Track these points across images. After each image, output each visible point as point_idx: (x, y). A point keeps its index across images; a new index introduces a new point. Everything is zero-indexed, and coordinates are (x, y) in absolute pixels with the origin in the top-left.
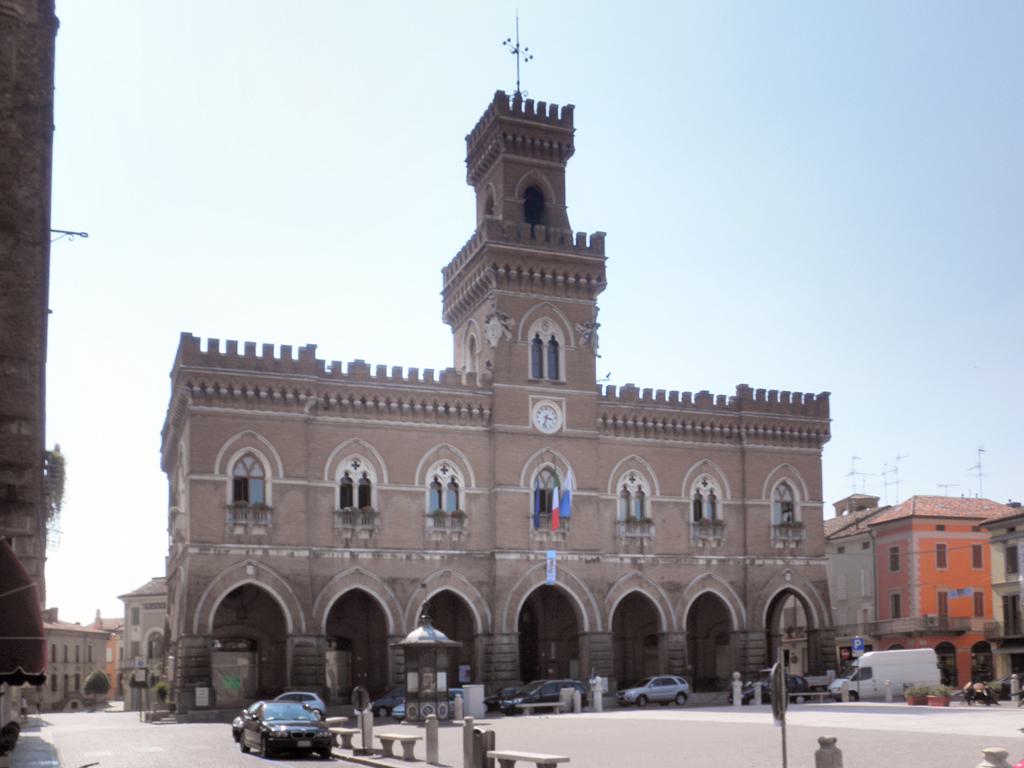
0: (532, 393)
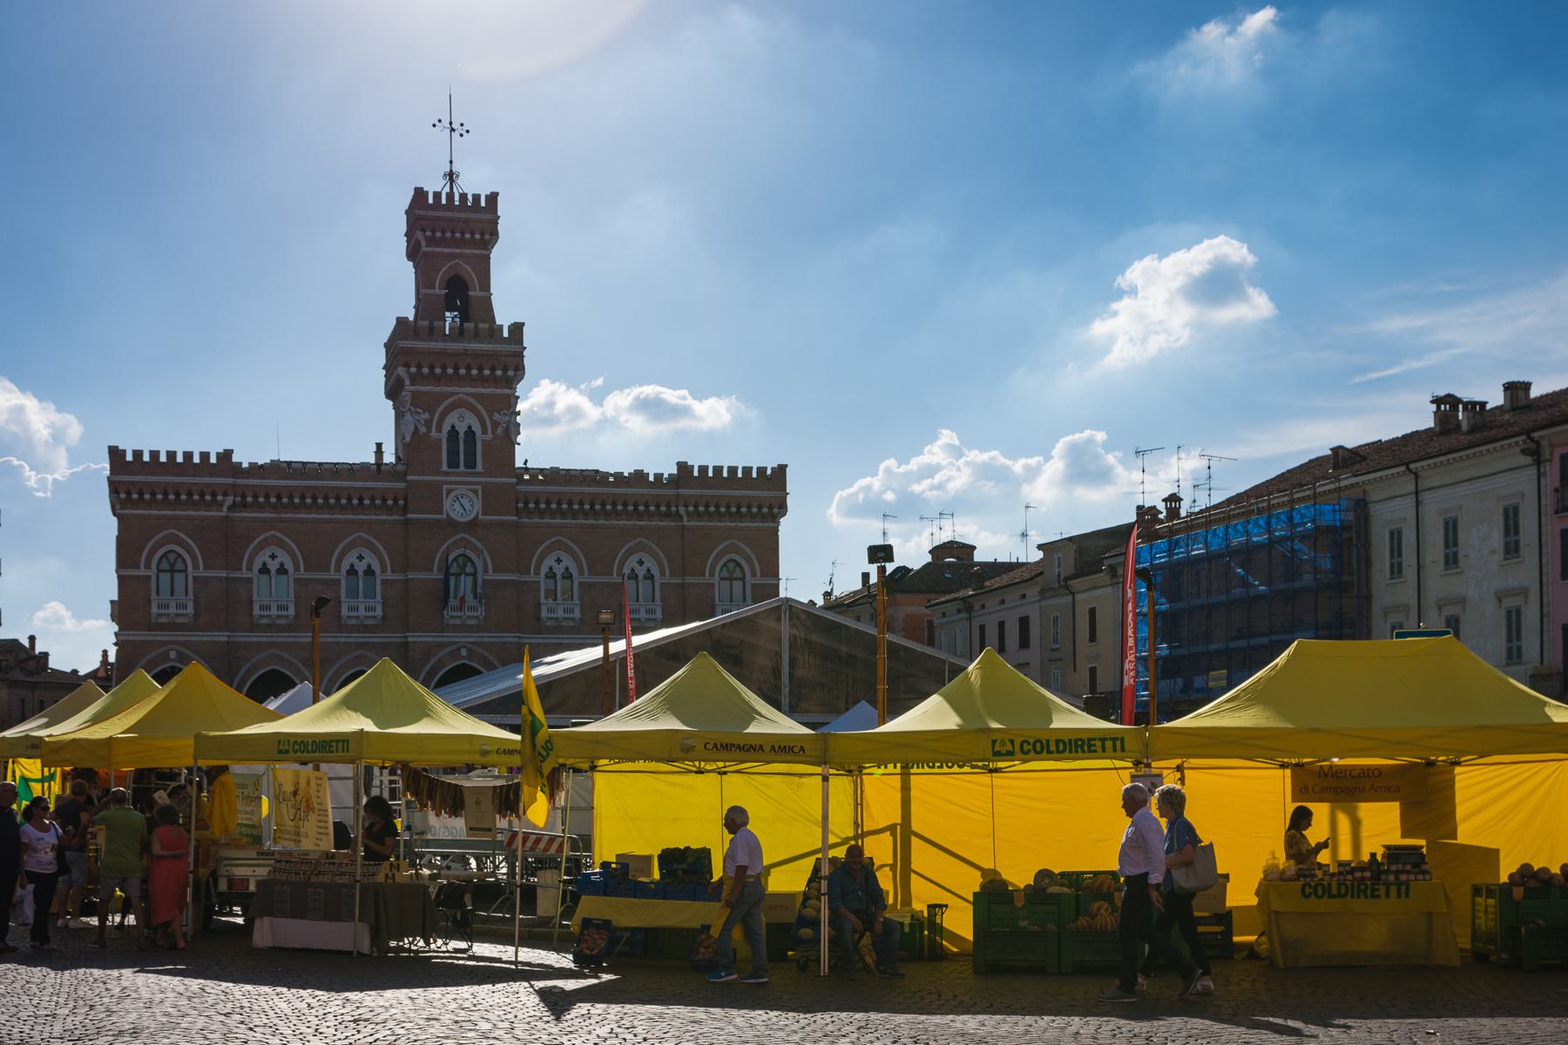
0: (447, 483)
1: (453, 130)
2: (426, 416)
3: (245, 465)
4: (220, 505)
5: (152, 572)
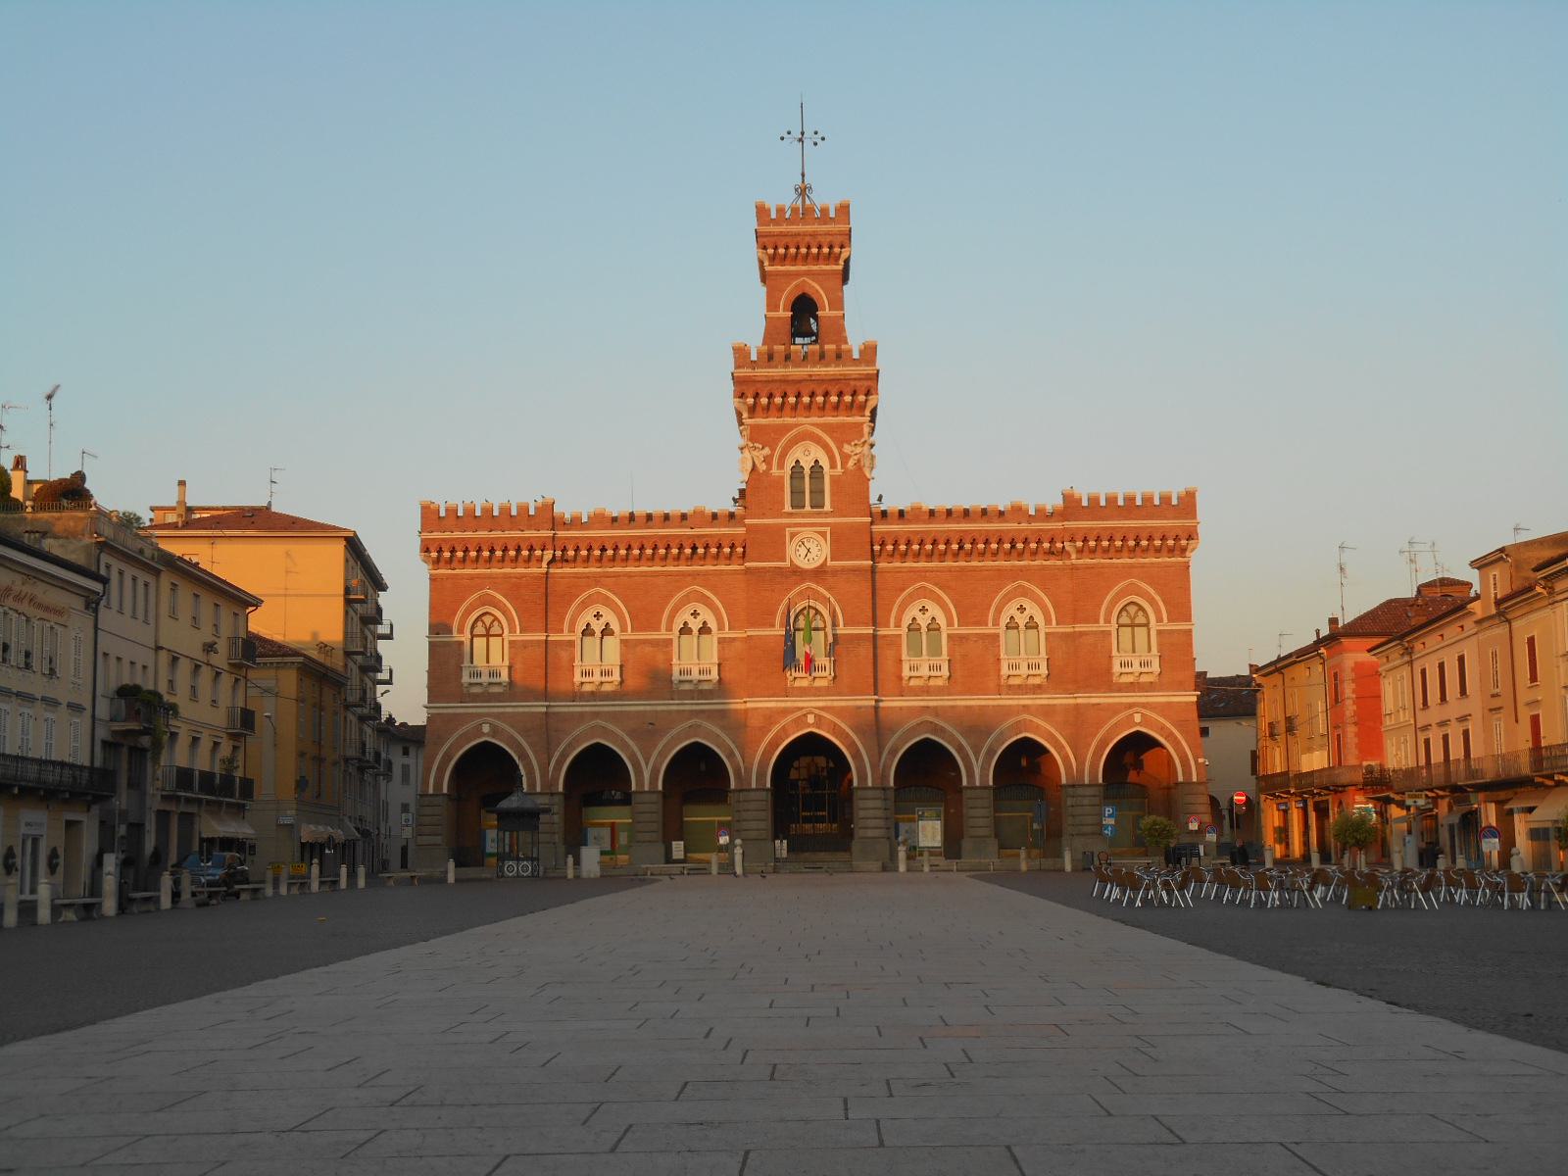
2: (767, 451)
3: (568, 516)
4: (540, 560)
5: (466, 638)
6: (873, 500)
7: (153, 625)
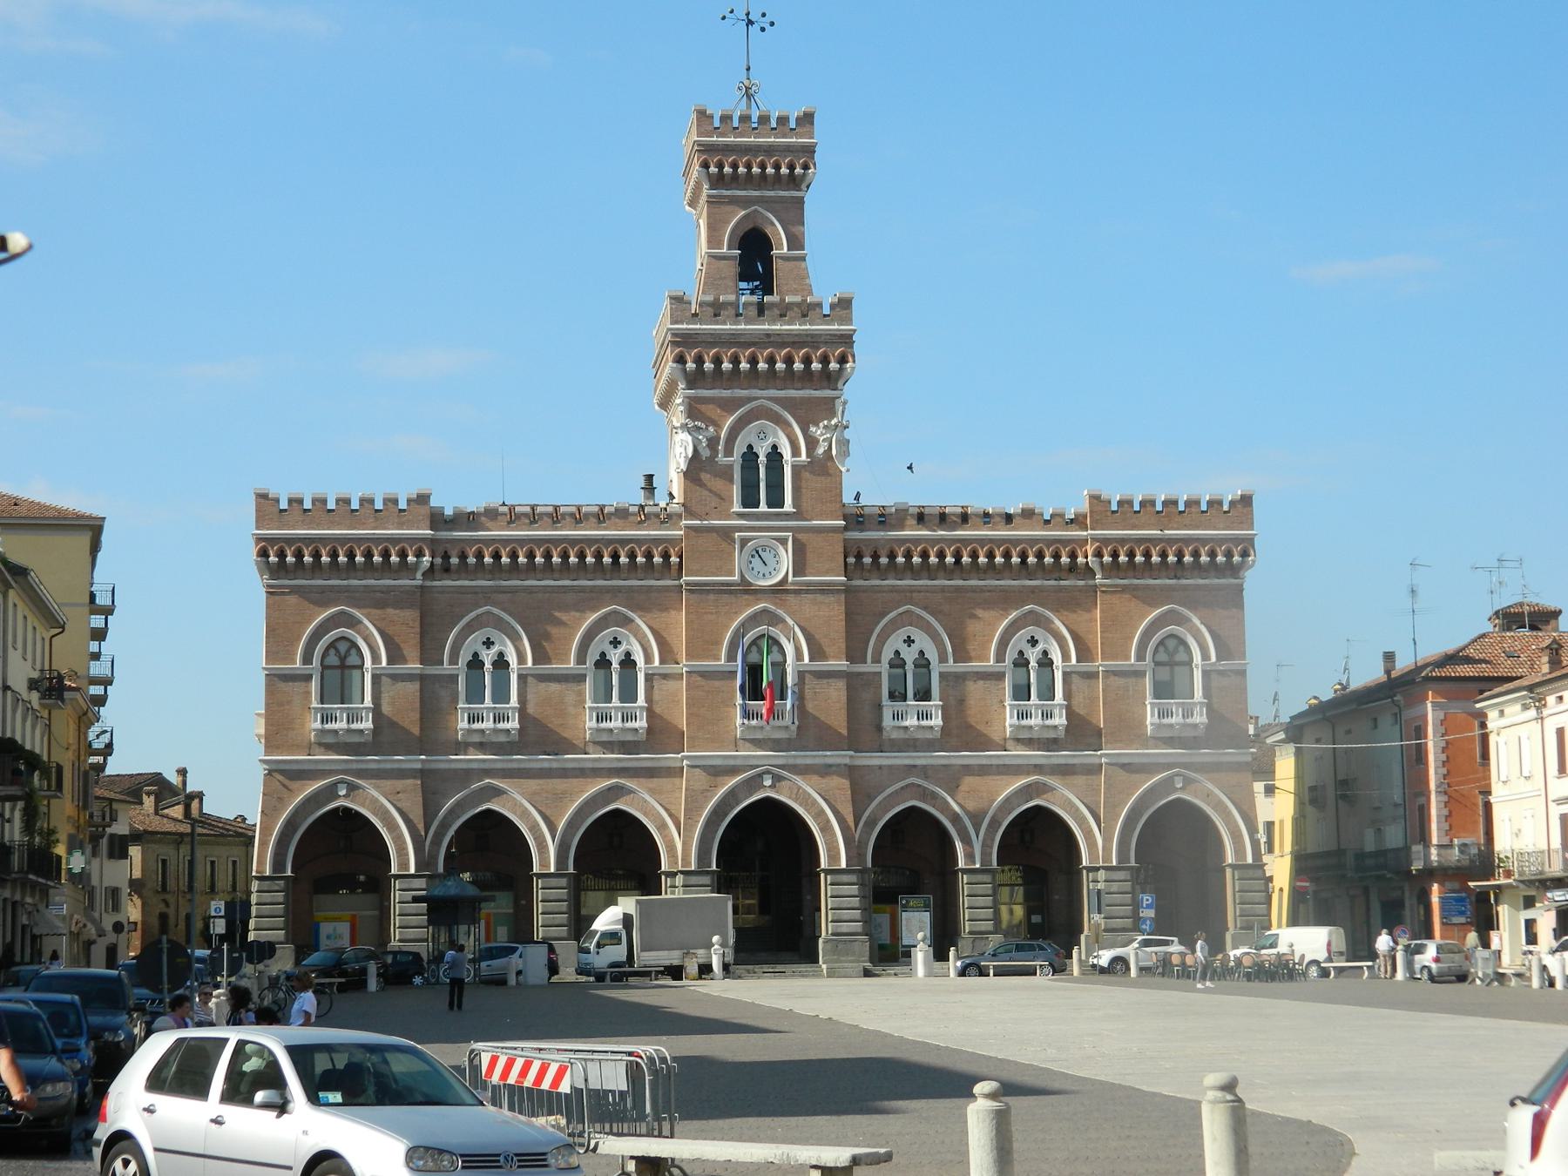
1: (750, 22)
3: (449, 512)
5: (884, 668)
6: (848, 498)
7: (20, 650)
